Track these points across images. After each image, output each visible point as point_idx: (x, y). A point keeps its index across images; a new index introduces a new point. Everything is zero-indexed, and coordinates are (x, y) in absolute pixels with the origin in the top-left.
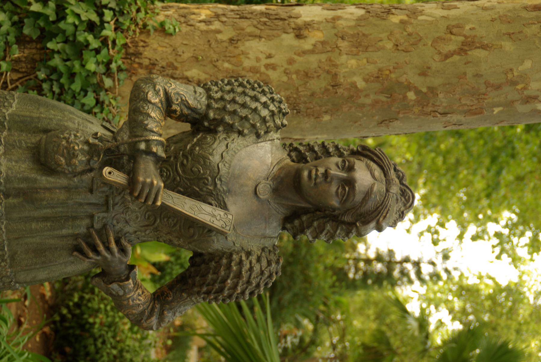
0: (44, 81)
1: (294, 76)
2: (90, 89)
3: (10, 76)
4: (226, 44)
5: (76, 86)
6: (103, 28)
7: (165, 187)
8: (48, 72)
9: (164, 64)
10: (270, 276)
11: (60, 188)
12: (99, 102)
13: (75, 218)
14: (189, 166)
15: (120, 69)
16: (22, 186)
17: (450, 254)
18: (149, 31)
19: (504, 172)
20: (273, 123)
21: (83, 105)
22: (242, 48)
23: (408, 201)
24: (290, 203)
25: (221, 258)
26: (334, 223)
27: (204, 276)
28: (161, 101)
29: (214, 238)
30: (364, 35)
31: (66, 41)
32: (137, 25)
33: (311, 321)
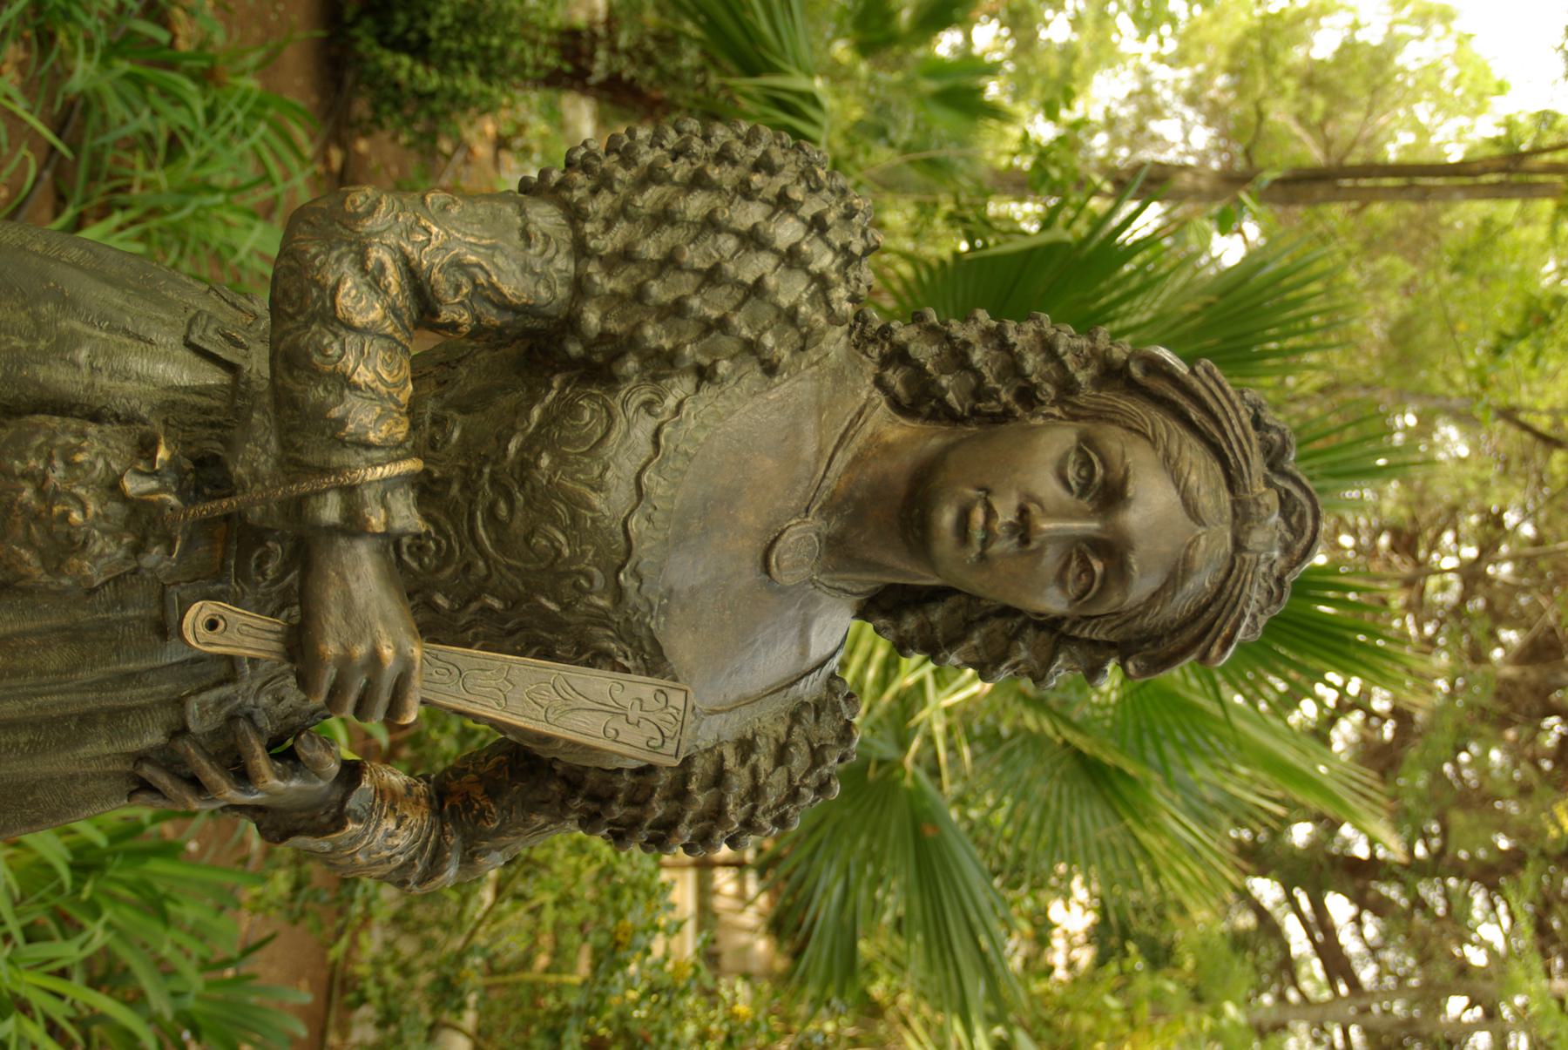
14: (518, 525)
20: (823, 310)
26: (1044, 635)
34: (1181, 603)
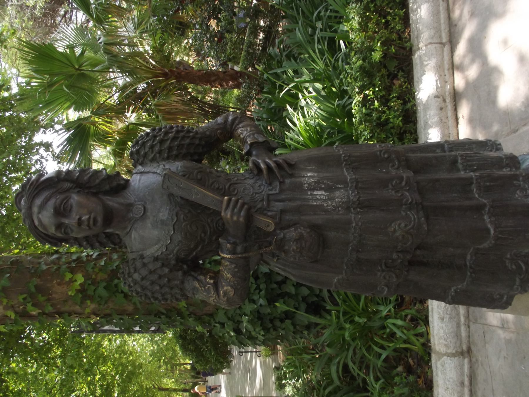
34: (45, 194)
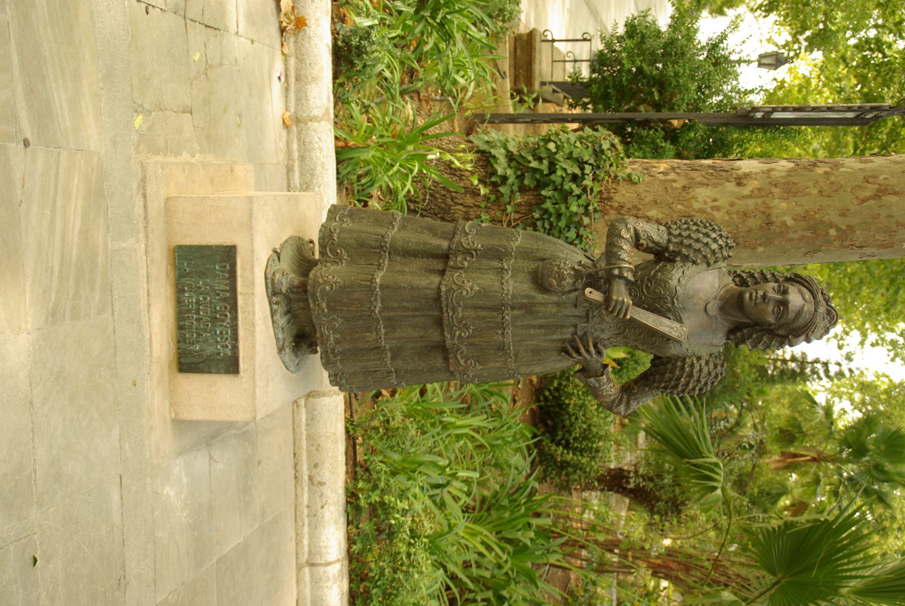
0: (538, 220)
1: (735, 216)
2: (572, 226)
3: (513, 216)
4: (679, 191)
5: (562, 224)
6: (584, 179)
7: (633, 304)
8: (541, 212)
9: (630, 206)
10: (716, 376)
11: (552, 304)
12: (579, 236)
13: (562, 327)
14: (653, 288)
15: (595, 211)
16: (524, 301)
17: (853, 357)
18: (619, 181)
19: (901, 292)
21: (567, 238)
22: (692, 194)
23: (832, 319)
24: (734, 319)
25: (676, 361)
27: (663, 374)
28: (631, 237)
29: (672, 345)
30: (793, 183)
31: (555, 190)
32: (610, 176)
33: (736, 407)
